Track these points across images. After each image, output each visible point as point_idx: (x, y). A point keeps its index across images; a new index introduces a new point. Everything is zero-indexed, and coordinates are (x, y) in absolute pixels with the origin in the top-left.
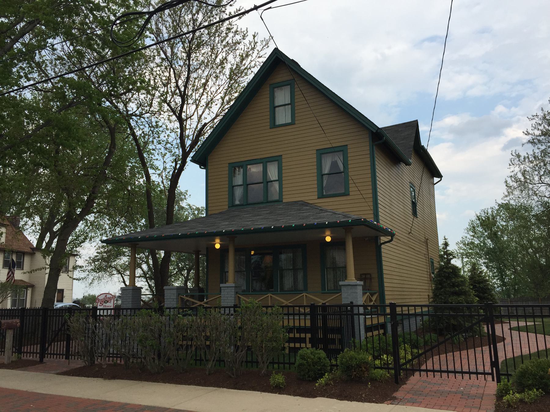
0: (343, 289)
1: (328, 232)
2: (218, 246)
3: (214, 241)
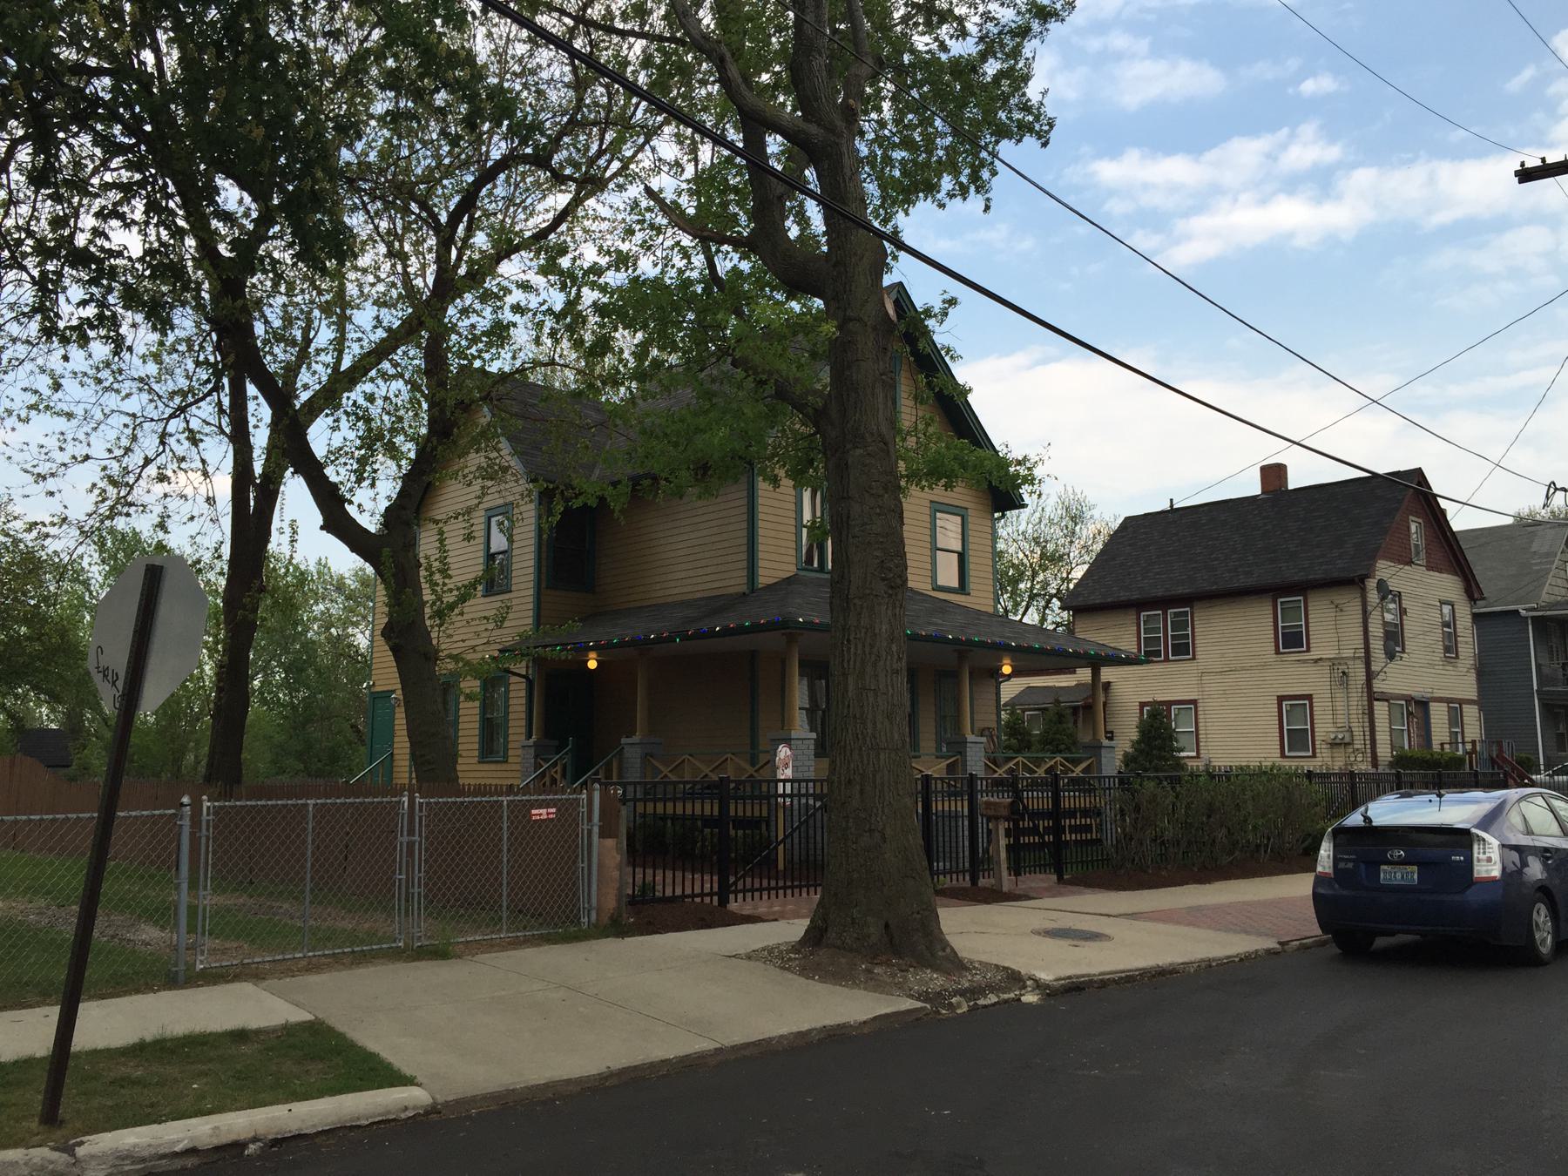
0: (1103, 751)
2: (592, 665)
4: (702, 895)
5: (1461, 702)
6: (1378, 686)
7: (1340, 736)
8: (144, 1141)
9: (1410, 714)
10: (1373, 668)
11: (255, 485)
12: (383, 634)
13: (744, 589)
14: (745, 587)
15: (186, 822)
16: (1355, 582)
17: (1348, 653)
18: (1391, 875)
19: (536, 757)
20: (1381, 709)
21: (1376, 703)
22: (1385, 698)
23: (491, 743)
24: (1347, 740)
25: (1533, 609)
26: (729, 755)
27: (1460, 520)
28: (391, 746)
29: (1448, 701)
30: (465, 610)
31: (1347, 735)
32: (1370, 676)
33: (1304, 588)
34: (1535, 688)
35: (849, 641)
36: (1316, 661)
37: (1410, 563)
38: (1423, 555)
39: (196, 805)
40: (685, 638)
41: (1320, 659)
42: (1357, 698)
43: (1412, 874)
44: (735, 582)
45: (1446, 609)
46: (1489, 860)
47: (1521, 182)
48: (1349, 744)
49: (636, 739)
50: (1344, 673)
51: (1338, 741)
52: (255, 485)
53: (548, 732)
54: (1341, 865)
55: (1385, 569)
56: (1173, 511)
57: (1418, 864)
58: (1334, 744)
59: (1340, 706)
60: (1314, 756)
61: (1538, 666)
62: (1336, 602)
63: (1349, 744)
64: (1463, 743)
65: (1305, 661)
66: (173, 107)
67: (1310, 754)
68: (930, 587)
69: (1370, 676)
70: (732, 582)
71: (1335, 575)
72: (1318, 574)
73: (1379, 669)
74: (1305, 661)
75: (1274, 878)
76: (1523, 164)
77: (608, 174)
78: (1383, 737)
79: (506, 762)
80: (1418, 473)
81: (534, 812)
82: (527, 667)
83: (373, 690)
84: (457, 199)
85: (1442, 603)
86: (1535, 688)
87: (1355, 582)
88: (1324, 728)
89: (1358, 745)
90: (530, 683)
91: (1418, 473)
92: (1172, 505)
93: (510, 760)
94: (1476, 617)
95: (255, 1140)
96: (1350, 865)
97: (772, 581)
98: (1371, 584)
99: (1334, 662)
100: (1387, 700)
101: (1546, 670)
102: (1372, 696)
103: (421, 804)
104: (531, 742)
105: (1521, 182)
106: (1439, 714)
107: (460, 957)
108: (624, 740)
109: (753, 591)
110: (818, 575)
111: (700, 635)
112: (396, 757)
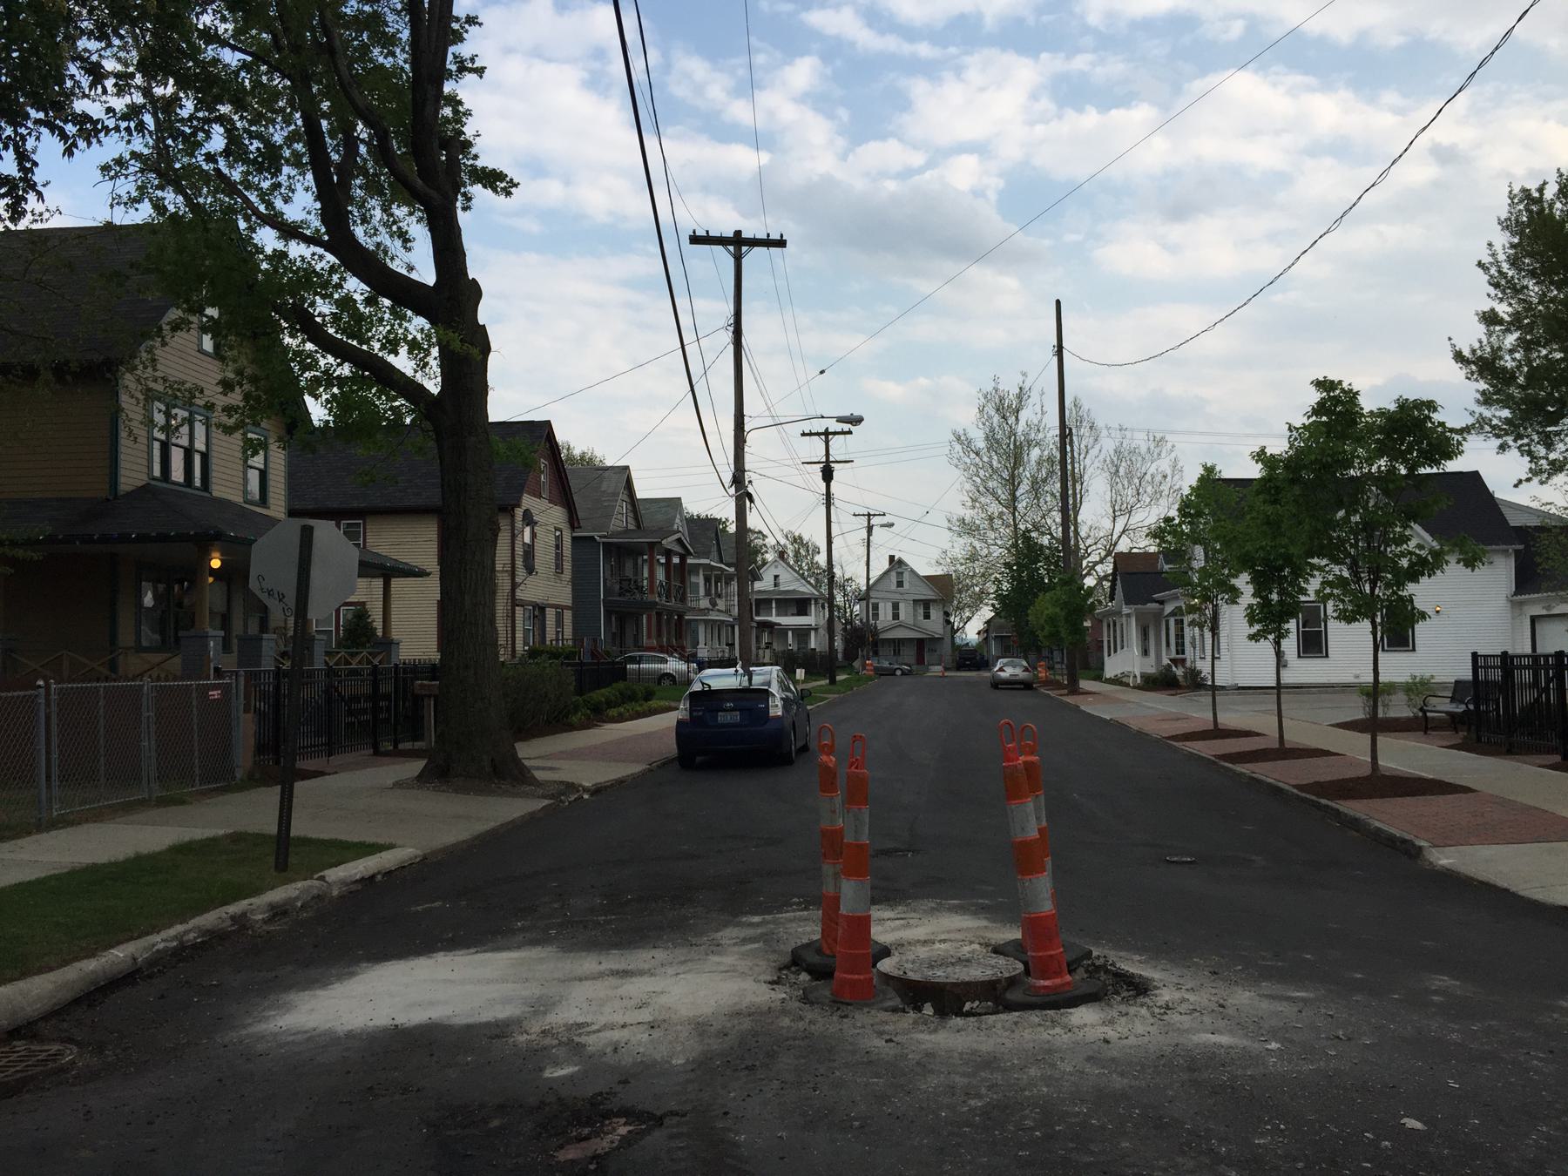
4: (307, 747)
5: (563, 608)
6: (519, 594)
8: (361, 868)
9: (535, 617)
15: (42, 701)
18: (723, 718)
20: (519, 611)
21: (517, 608)
22: (523, 604)
23: (649, 637)
25: (605, 537)
29: (555, 606)
32: (514, 586)
35: (465, 570)
37: (540, 497)
38: (547, 491)
39: (47, 686)
43: (736, 717)
45: (558, 533)
46: (777, 706)
47: (691, 243)
54: (695, 714)
55: (527, 501)
57: (740, 710)
64: (563, 640)
66: (178, 166)
68: (242, 500)
69: (514, 586)
75: (557, 735)
76: (694, 232)
77: (1115, 537)
78: (519, 635)
81: (211, 693)
84: (1060, 529)
85: (556, 529)
91: (548, 423)
94: (574, 539)
95: (379, 873)
96: (700, 713)
98: (519, 512)
100: (523, 606)
101: (608, 584)
105: (691, 243)
106: (550, 614)
107: (191, 803)
110: (159, 484)
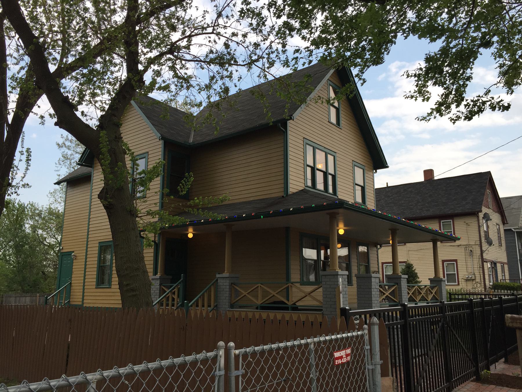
1: (191, 230)
2: (190, 236)
3: (188, 231)
7: (470, 277)
10: (483, 249)
11: (8, 125)
12: (100, 196)
13: (282, 194)
14: (283, 193)
16: (474, 214)
17: (472, 243)
19: (161, 285)
24: (473, 278)
25: (517, 229)
26: (259, 285)
27: (502, 194)
28: (71, 279)
30: (151, 187)
31: (473, 276)
32: (482, 252)
33: (452, 216)
34: (519, 259)
36: (458, 246)
40: (267, 215)
41: (460, 245)
42: (477, 262)
44: (276, 192)
48: (474, 280)
49: (226, 274)
50: (471, 251)
51: (469, 279)
52: (8, 125)
53: (166, 271)
56: (388, 187)
58: (467, 280)
59: (469, 264)
60: (459, 284)
61: (519, 250)
62: (467, 222)
63: (474, 280)
65: (454, 246)
67: (457, 284)
69: (482, 252)
70: (273, 191)
71: (467, 211)
72: (459, 211)
73: (485, 250)
74: (454, 246)
79: (111, 288)
80: (489, 173)
81: (337, 355)
82: (155, 237)
83: (62, 251)
86: (519, 259)
87: (474, 214)
88: (463, 273)
89: (478, 280)
90: (157, 245)
91: (489, 173)
92: (387, 185)
93: (112, 287)
94: (505, 230)
97: (295, 191)
98: (481, 215)
99: (467, 246)
102: (483, 261)
103: (237, 357)
104: (158, 276)
108: (218, 276)
109: (287, 196)
111: (277, 214)
112: (73, 285)
